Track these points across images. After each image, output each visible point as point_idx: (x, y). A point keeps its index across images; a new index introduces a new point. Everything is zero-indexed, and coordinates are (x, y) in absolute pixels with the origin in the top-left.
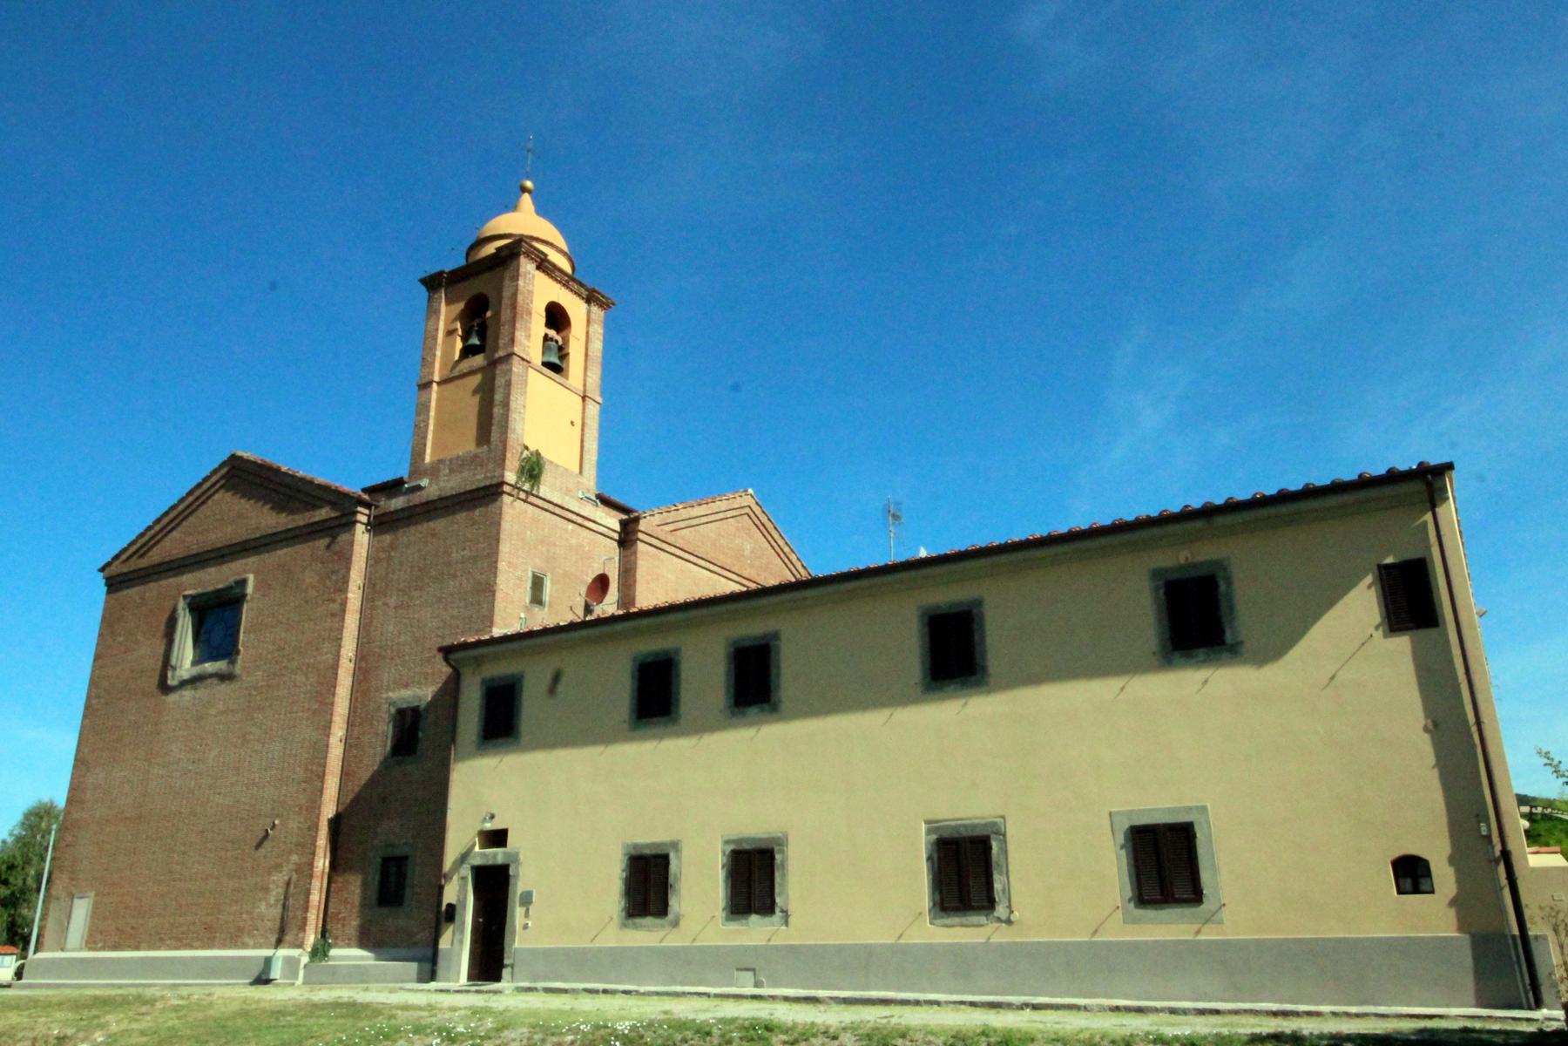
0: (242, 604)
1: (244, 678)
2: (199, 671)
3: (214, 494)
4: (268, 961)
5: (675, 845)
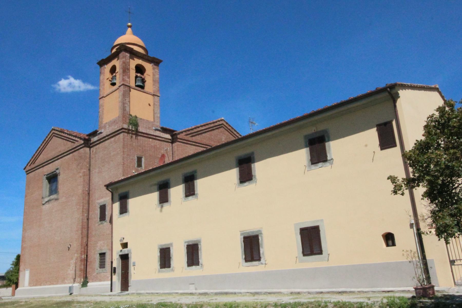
5: (171, 244)
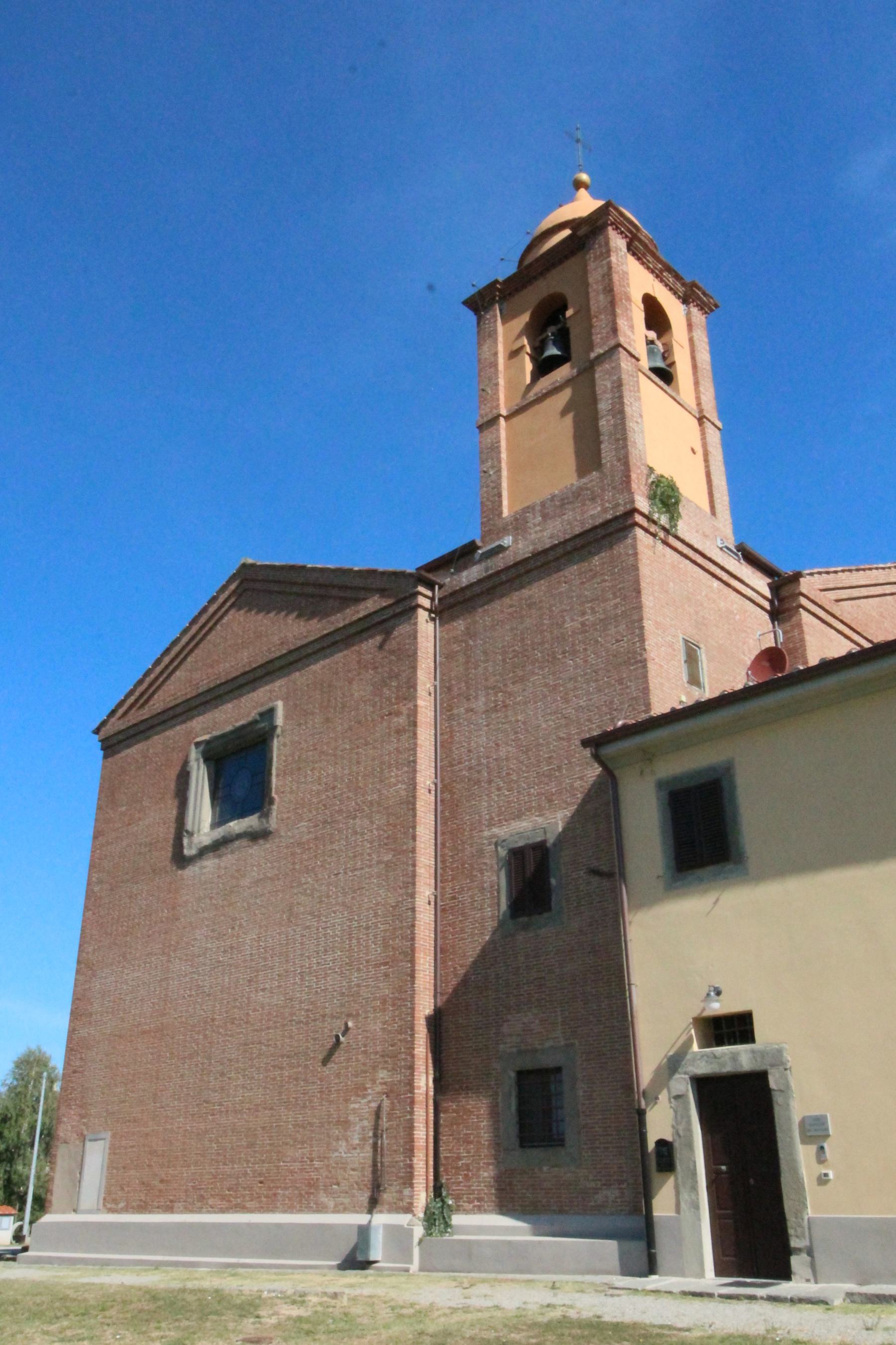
0: (272, 739)
1: (283, 834)
2: (222, 834)
3: (222, 617)
4: (364, 1232)
